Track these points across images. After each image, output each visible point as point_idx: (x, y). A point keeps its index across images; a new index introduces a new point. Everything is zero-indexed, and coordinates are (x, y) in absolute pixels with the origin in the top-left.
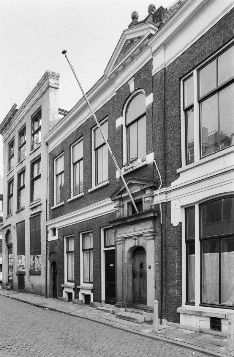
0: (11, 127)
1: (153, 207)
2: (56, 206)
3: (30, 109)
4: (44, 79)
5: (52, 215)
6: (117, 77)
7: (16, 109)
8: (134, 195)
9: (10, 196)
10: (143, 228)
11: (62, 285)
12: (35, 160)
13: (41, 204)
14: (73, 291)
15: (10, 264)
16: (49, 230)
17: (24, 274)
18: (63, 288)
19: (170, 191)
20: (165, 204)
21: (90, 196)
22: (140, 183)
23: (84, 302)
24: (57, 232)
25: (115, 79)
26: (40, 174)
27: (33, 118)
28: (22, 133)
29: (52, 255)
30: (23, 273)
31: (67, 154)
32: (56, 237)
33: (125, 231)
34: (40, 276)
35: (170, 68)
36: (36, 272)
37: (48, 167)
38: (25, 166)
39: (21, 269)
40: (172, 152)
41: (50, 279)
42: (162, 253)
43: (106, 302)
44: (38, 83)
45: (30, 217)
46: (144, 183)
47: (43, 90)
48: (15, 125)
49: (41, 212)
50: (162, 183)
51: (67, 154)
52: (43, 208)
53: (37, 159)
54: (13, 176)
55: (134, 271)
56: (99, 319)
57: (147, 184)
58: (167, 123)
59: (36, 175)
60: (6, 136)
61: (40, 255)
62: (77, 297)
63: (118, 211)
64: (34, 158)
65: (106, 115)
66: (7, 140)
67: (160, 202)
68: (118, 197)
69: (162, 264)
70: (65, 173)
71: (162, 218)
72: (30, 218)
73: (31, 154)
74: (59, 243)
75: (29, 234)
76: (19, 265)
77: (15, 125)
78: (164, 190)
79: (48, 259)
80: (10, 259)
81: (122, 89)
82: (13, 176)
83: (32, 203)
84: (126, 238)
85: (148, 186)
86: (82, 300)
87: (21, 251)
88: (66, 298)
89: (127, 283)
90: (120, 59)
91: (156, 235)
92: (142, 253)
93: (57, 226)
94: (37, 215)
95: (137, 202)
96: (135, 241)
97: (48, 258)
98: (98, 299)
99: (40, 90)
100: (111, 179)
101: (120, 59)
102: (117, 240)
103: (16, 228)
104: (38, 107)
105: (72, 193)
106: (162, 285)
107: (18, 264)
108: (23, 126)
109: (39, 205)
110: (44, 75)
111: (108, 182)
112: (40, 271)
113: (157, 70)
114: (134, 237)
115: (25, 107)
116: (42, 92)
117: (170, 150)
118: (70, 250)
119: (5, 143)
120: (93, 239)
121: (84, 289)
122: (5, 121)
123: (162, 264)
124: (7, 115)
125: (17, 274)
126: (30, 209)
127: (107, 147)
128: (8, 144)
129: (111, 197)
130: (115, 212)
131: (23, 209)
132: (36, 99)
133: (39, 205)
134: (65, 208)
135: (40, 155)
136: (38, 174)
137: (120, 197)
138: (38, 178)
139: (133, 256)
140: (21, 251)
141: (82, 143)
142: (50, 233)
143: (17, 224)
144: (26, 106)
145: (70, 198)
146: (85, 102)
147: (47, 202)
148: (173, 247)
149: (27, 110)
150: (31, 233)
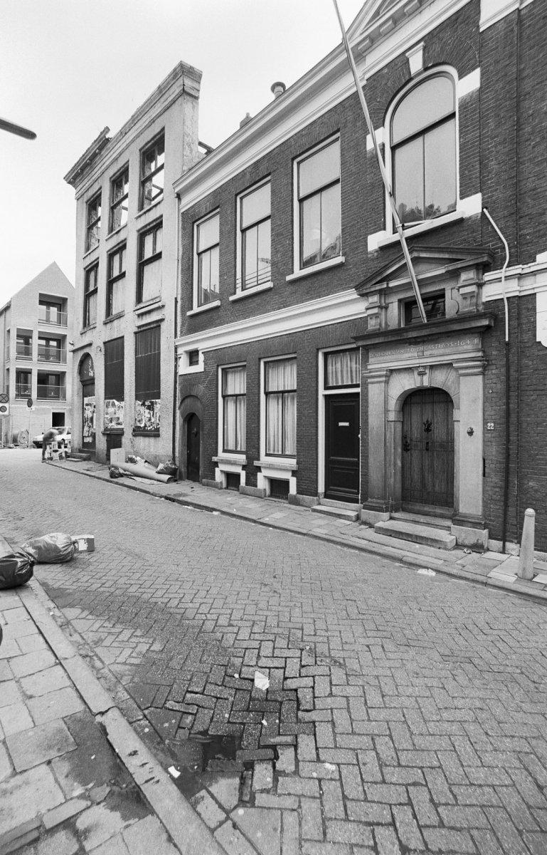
0: (93, 173)
1: (481, 308)
2: (196, 310)
3: (137, 136)
4: (174, 78)
5: (190, 325)
6: (395, 30)
7: (107, 137)
8: (422, 283)
9: (89, 294)
10: (441, 351)
11: (215, 459)
12: (148, 227)
13: (163, 306)
14: (242, 470)
15: (88, 414)
16: (181, 354)
17: (122, 434)
18: (216, 464)
19: (534, 273)
20: (518, 300)
21: (289, 289)
22: (447, 256)
23: (268, 492)
24: (201, 357)
25: (364, 54)
26: (123, 271)
27: (144, 153)
28: (119, 180)
29: (188, 401)
30: (119, 432)
31: (229, 212)
32: (199, 368)
33: (395, 357)
34: (157, 439)
35: (535, 8)
36: (147, 431)
37: (180, 239)
38: (125, 239)
39: (113, 425)
40: (539, 190)
41: (182, 445)
42: (508, 404)
43: (326, 496)
44: (159, 87)
45: (136, 330)
46: (459, 257)
47: (170, 99)
48: (103, 168)
49: (162, 320)
50: (510, 256)
51: (229, 212)
52: (168, 313)
53: (151, 225)
54: (98, 258)
55: (406, 438)
56: (338, 535)
57: (469, 258)
58: (524, 129)
59: (116, 273)
60: (82, 190)
61: (157, 400)
62: (251, 481)
63: (376, 316)
64: (147, 223)
65: (335, 129)
66: (85, 195)
67: (505, 296)
68: (378, 287)
69: (508, 427)
70: (224, 247)
71: (509, 330)
72: (136, 333)
73: (140, 216)
74: (208, 378)
75: (133, 361)
76: (108, 416)
77: (103, 168)
78: (517, 269)
79: (177, 408)
80: (87, 405)
81: (386, 71)
82: (98, 258)
83: (142, 305)
84: (392, 371)
85: (471, 263)
86: (265, 489)
87: (115, 390)
88: (221, 483)
89: (394, 463)
90: (385, 9)
91: (488, 365)
92: (429, 403)
93: (201, 346)
94: (152, 326)
95: (426, 296)
96: (419, 378)
97: (178, 405)
98: (307, 487)
99: (162, 100)
100: (348, 253)
101: (385, 9)
102: (371, 374)
103: (103, 350)
104: (158, 130)
105: (239, 285)
106: (507, 471)
107: (106, 416)
108: (121, 168)
109: (159, 308)
110: (175, 70)
111: (270, 285)
112: (158, 430)
113: (488, 20)
114: (421, 370)
115: (126, 134)
116: (166, 103)
117: (530, 185)
118: (230, 392)
119: (79, 202)
120: (297, 372)
121: (271, 467)
122: (84, 160)
123: (508, 427)
124: (89, 149)
125: (104, 434)
126: (137, 316)
127: (216, 253)
128: (86, 203)
129: (357, 288)
130: (365, 320)
131: (121, 317)
132: (153, 116)
133: (159, 308)
134: (221, 312)
135: (161, 216)
136: (153, 253)
137: (385, 286)
138: (122, 278)
139: (403, 408)
140: (115, 390)
141: (269, 186)
142: (184, 361)
143: (105, 343)
144: (130, 132)
145: (235, 293)
146: (345, 56)
147: (176, 302)
148: (538, 392)
149: (131, 138)
150: (137, 360)
